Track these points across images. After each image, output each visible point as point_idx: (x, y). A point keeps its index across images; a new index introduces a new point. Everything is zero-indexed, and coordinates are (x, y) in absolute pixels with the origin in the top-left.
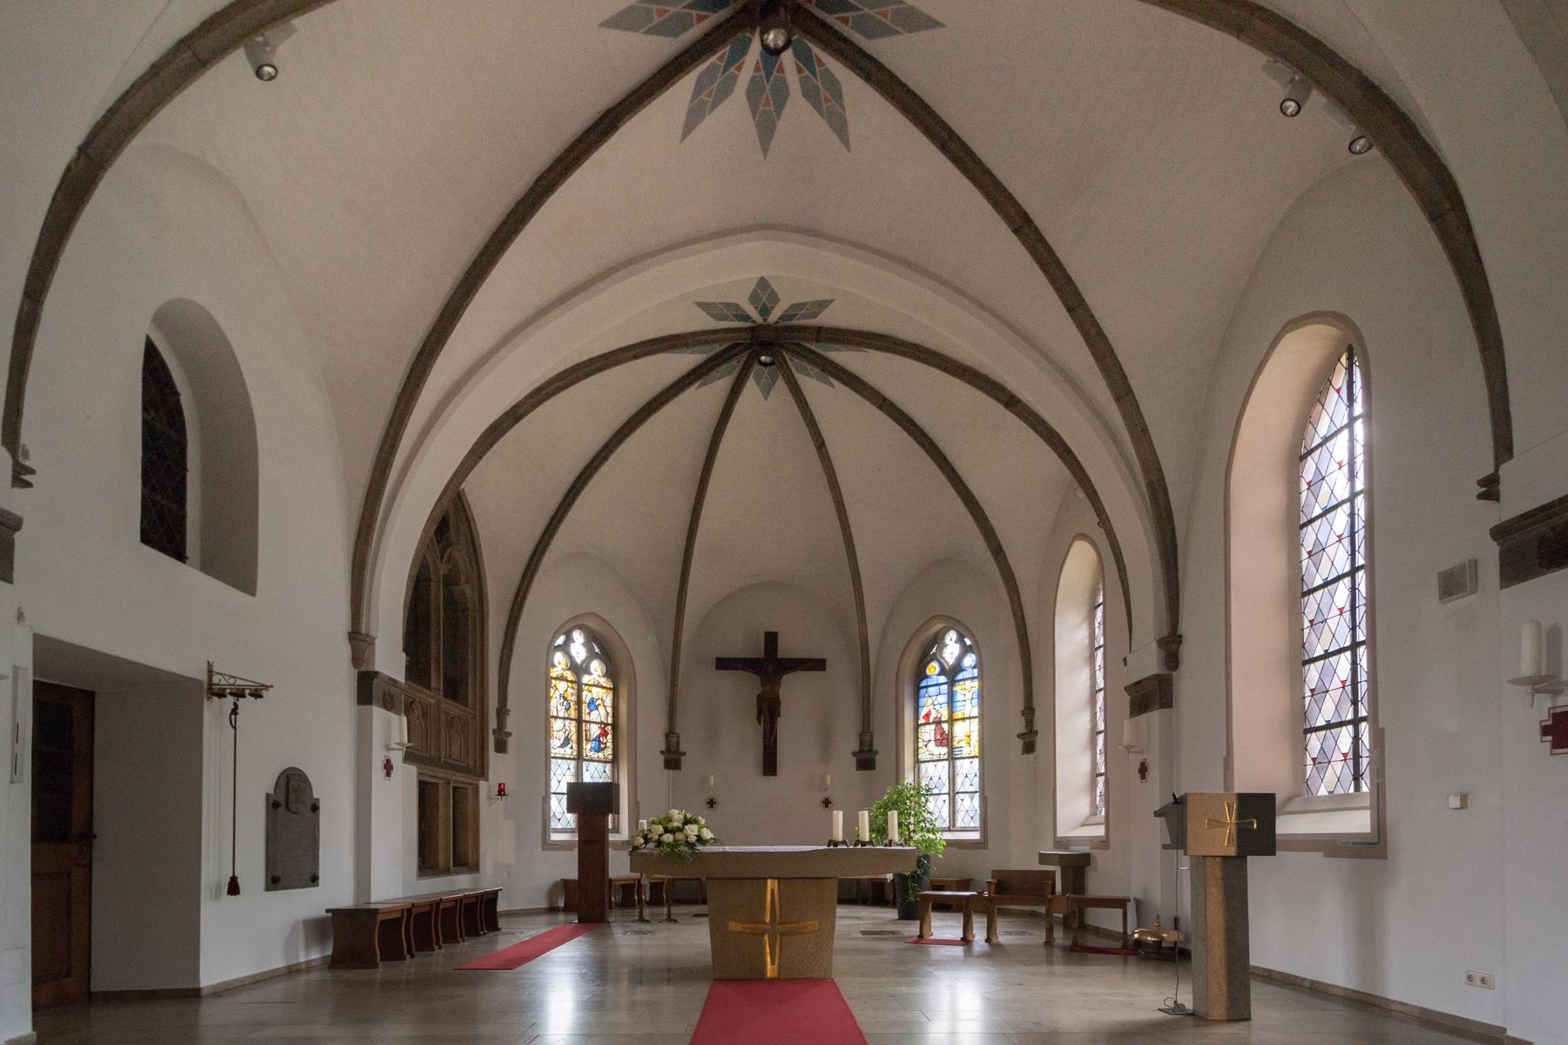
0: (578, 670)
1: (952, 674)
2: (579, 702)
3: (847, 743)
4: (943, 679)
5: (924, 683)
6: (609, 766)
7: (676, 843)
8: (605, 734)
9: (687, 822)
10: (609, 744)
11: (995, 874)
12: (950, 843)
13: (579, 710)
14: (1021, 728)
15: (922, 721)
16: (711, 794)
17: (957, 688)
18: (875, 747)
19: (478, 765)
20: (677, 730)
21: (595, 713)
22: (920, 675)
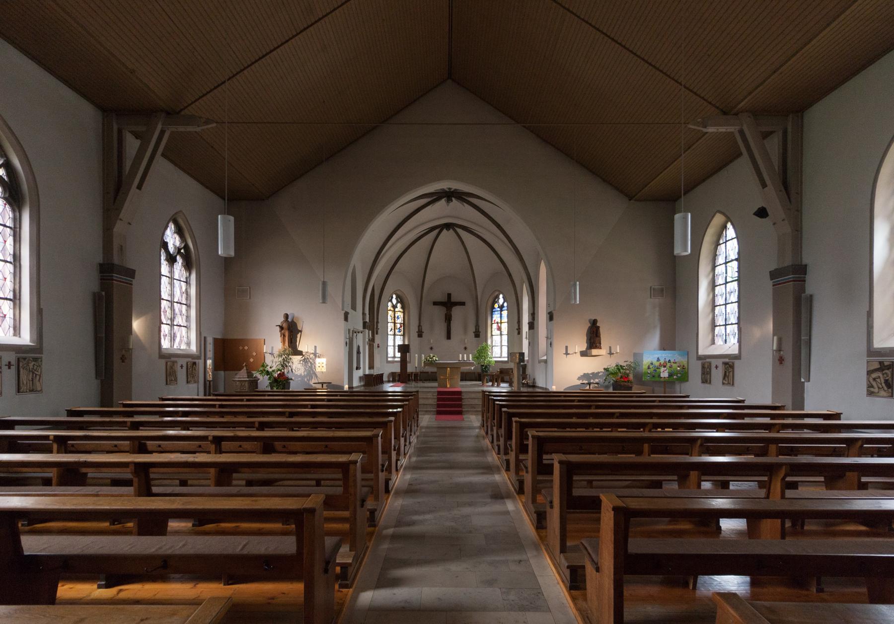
0: (394, 307)
1: (501, 307)
2: (395, 317)
3: (472, 329)
4: (499, 309)
5: (494, 310)
6: (402, 337)
7: (432, 361)
8: (401, 327)
9: (433, 356)
10: (402, 330)
11: (500, 369)
12: (496, 361)
13: (395, 320)
14: (517, 327)
15: (493, 322)
16: (432, 346)
17: (502, 313)
18: (480, 330)
19: (18, 229)
20: (421, 325)
21: (398, 320)
22: (493, 308)
